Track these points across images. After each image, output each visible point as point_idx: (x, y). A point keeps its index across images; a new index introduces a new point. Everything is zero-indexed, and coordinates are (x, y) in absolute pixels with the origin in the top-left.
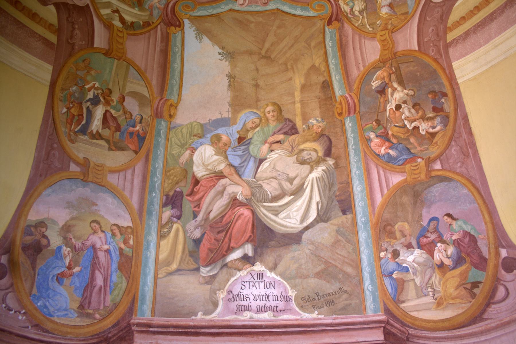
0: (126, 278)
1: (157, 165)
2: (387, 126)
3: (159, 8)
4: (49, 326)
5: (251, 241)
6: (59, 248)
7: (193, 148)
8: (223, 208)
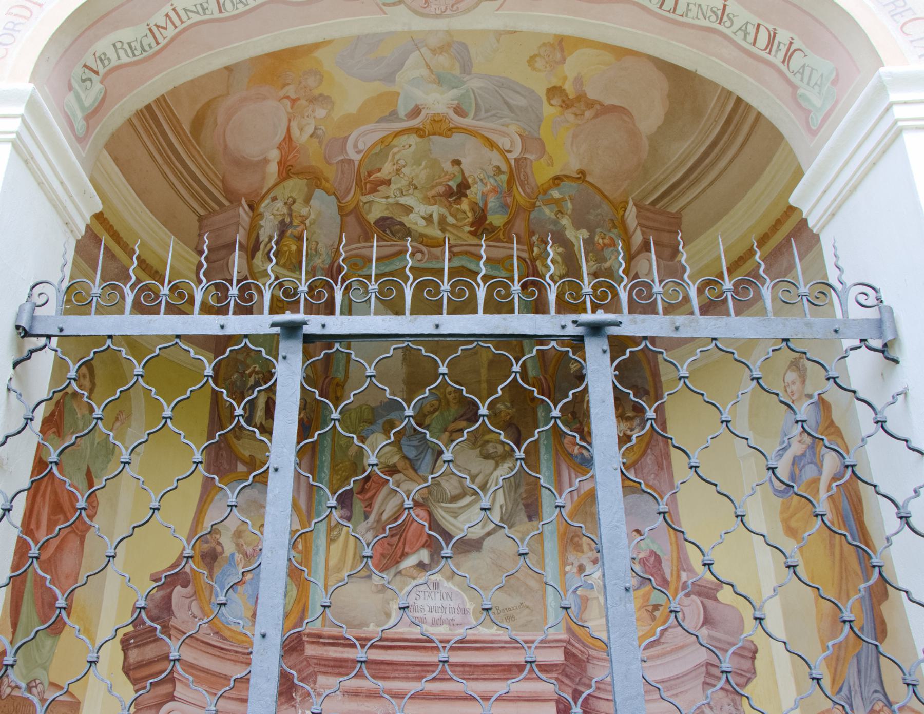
0: (296, 585)
1: (324, 458)
2: (583, 420)
3: (323, 269)
4: (227, 634)
5: (427, 547)
6: (233, 555)
7: (363, 436)
8: (397, 508)
